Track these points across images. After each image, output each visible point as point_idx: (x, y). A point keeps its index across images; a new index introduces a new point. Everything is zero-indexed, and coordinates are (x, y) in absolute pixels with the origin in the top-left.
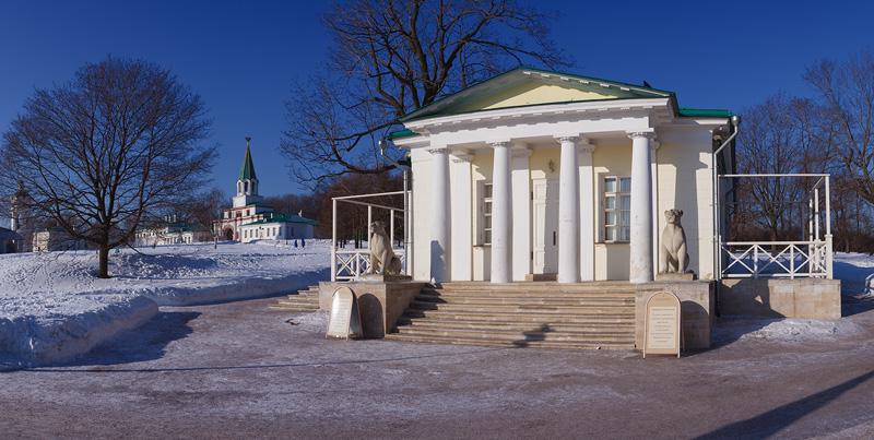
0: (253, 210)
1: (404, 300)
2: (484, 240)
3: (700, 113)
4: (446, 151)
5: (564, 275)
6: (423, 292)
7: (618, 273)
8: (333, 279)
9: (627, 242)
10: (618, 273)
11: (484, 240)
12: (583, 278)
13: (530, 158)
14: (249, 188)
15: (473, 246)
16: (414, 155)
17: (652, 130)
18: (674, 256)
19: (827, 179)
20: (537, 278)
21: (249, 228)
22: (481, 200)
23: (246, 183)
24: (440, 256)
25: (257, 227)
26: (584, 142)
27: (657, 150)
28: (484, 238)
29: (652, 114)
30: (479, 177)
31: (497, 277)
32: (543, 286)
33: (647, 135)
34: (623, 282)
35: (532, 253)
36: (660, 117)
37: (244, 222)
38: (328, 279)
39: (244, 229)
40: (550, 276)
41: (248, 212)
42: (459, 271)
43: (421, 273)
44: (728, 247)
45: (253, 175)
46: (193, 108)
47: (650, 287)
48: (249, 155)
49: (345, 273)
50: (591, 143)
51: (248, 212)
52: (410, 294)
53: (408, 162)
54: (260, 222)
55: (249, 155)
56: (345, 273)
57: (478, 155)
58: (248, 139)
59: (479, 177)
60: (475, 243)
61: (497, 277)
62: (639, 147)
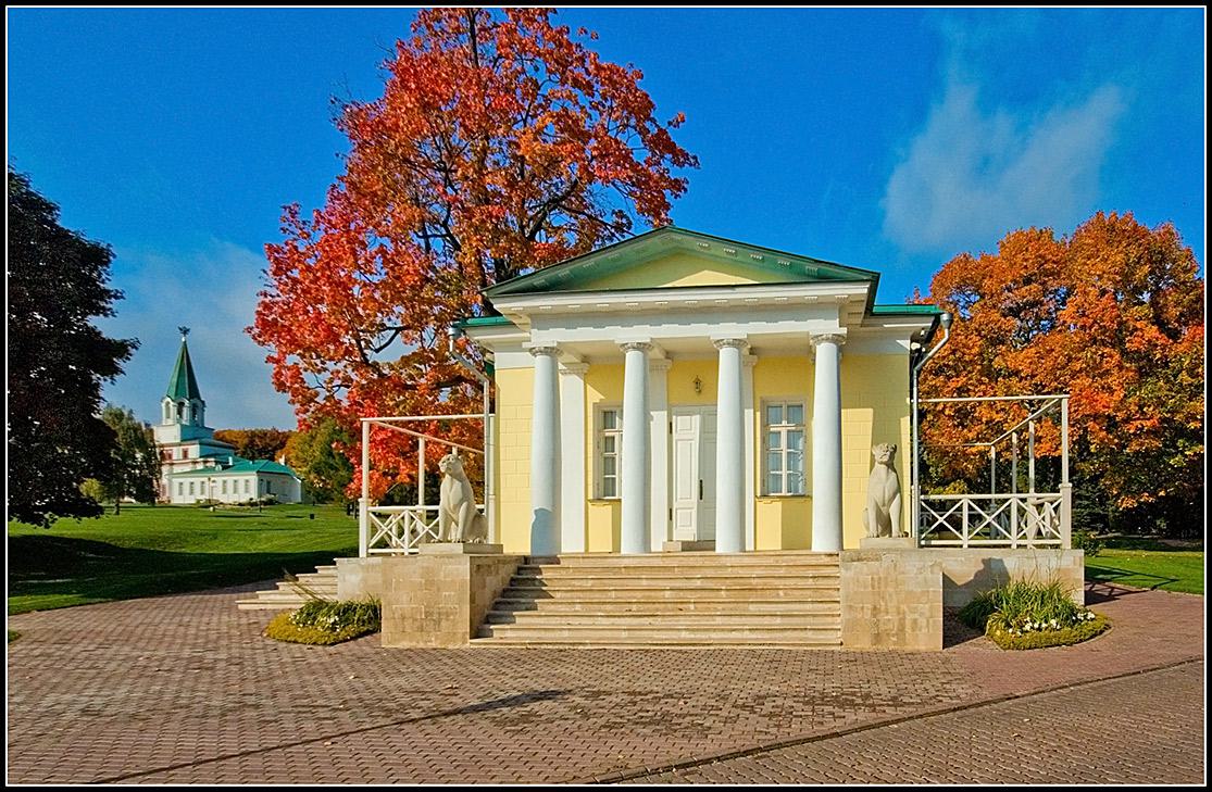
0: (194, 450)
1: (495, 582)
2: (606, 490)
3: (892, 310)
4: (551, 352)
5: (723, 545)
6: (519, 570)
7: (796, 537)
8: (362, 552)
9: (807, 497)
10: (796, 537)
11: (606, 490)
12: (747, 549)
13: (668, 372)
14: (186, 411)
15: (587, 500)
16: (501, 360)
17: (844, 331)
18: (884, 509)
19: (1065, 404)
20: (688, 546)
21: (187, 481)
22: (598, 431)
23: (181, 405)
24: (546, 522)
25: (197, 480)
26: (656, 353)
27: (754, 367)
28: (602, 490)
29: (841, 308)
30: (595, 396)
31: (629, 546)
32: (695, 558)
33: (836, 339)
34: (804, 552)
35: (671, 511)
36: (168, 417)
37: (177, 469)
38: (354, 552)
39: (176, 481)
40: (704, 544)
41: (185, 454)
42: (570, 542)
43: (517, 542)
44: (931, 504)
45: (194, 393)
46: (98, 256)
47: (645, 563)
48: (185, 356)
49: (383, 544)
50: (667, 358)
51: (185, 454)
52: (508, 571)
53: (489, 368)
54: (207, 469)
55: (185, 356)
56: (383, 544)
57: (600, 366)
58: (185, 331)
59: (595, 396)
60: (590, 497)
61: (629, 546)
62: (825, 355)
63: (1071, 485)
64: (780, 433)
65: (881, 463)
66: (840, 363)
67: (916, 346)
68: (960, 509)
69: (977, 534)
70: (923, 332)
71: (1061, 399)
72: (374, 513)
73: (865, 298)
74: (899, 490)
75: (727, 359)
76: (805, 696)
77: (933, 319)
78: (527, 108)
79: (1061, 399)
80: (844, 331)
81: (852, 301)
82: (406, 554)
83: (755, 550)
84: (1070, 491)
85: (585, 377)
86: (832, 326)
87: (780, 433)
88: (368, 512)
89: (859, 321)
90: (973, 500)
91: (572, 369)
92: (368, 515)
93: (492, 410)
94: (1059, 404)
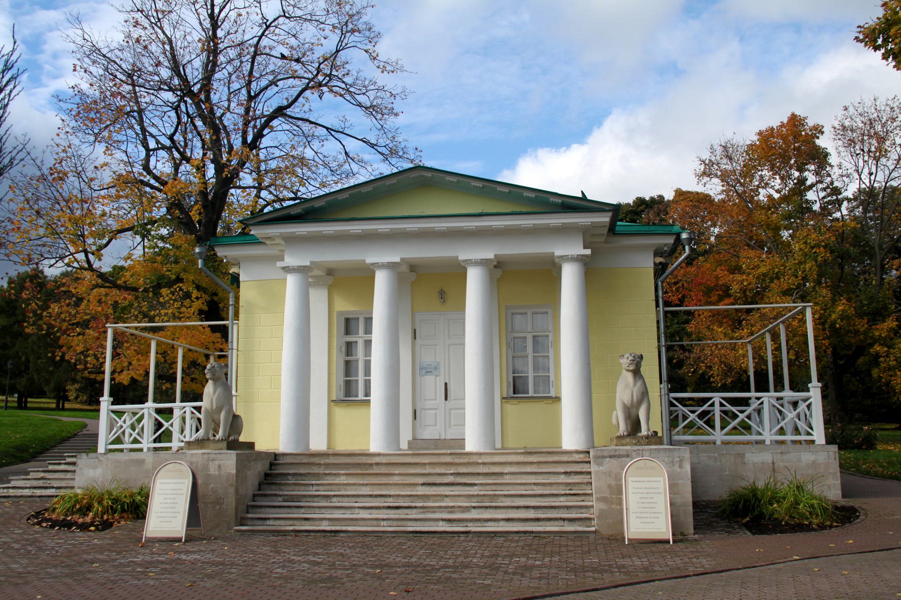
8: (101, 449)
17: (588, 252)
18: (633, 411)
26: (405, 268)
33: (580, 259)
63: (820, 385)
64: (525, 338)
65: (628, 371)
66: (586, 273)
67: (659, 260)
68: (712, 405)
69: (735, 428)
70: (665, 249)
71: (805, 307)
72: (723, 398)
73: (608, 225)
74: (645, 394)
75: (475, 280)
76: (567, 567)
77: (674, 237)
78: (307, 81)
79: (805, 307)
80: (588, 252)
81: (601, 225)
82: (718, 443)
83: (503, 448)
84: (819, 391)
85: (331, 290)
86: (578, 250)
87: (525, 338)
88: (108, 410)
89: (603, 240)
90: (723, 398)
91: (318, 282)
92: (108, 413)
93: (236, 315)
94: (802, 312)
